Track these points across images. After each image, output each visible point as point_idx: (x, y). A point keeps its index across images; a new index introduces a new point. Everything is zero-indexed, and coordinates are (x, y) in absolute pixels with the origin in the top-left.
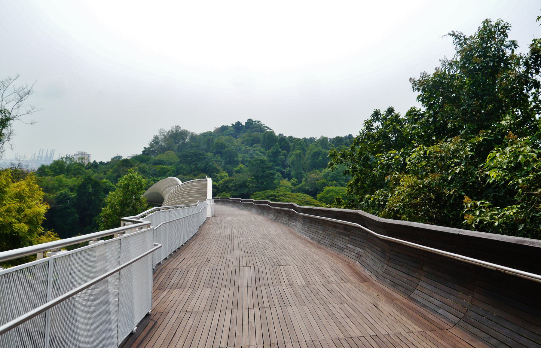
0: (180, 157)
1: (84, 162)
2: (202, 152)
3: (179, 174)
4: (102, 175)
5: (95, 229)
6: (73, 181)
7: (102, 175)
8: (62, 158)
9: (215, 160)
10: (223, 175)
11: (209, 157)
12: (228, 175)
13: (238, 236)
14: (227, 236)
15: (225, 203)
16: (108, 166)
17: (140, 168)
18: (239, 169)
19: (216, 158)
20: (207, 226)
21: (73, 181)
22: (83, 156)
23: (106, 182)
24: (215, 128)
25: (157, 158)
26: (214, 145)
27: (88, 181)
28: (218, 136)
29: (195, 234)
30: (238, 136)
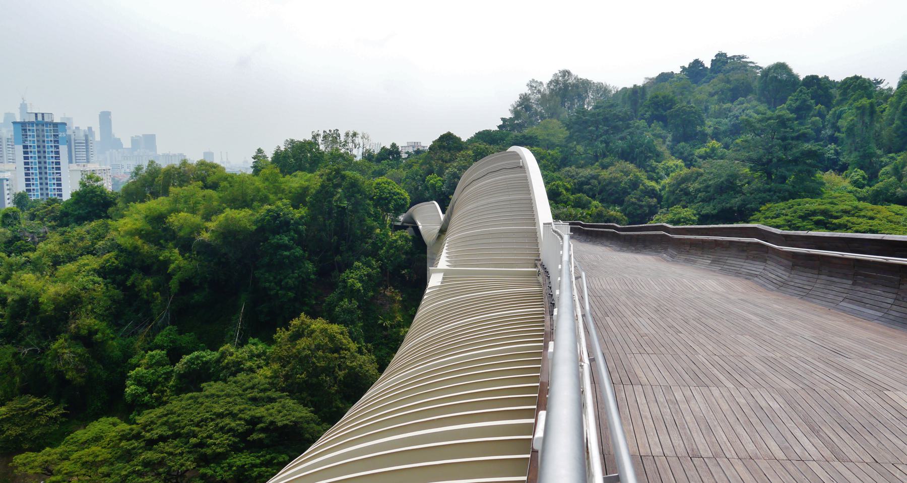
12: (683, 164)
18: (708, 150)
24: (646, 78)
26: (647, 102)
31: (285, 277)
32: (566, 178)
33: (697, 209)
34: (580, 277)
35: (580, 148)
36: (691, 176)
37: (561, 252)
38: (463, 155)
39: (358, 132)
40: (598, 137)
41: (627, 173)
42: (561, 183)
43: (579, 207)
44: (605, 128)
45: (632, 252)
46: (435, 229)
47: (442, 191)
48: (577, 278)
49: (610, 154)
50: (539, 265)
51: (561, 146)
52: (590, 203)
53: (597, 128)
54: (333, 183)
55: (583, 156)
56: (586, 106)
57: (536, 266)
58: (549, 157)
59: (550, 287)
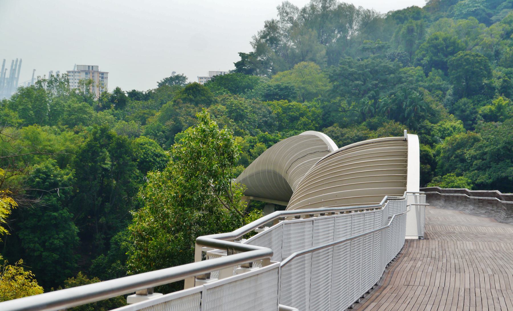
0: (332, 79)
1: (91, 91)
2: (391, 65)
3: (331, 124)
4: (134, 126)
5: (119, 262)
6: (66, 140)
7: (134, 126)
8: (39, 82)
9: (427, 84)
10: (448, 125)
11: (412, 76)
12: (461, 126)
13: (495, 295)
14: (462, 293)
15: (453, 201)
16: (149, 102)
17: (229, 107)
18: (493, 108)
19: (431, 81)
20: (406, 265)
21: (66, 140)
22: (90, 77)
23: (146, 143)
25: (273, 82)
26: (425, 44)
27: (103, 141)
28: (436, 19)
29: (376, 285)
30: (493, 18)
31: (50, 238)
33: (472, 178)
36: (467, 142)
53: (365, 81)
54: (99, 143)
58: (310, 114)
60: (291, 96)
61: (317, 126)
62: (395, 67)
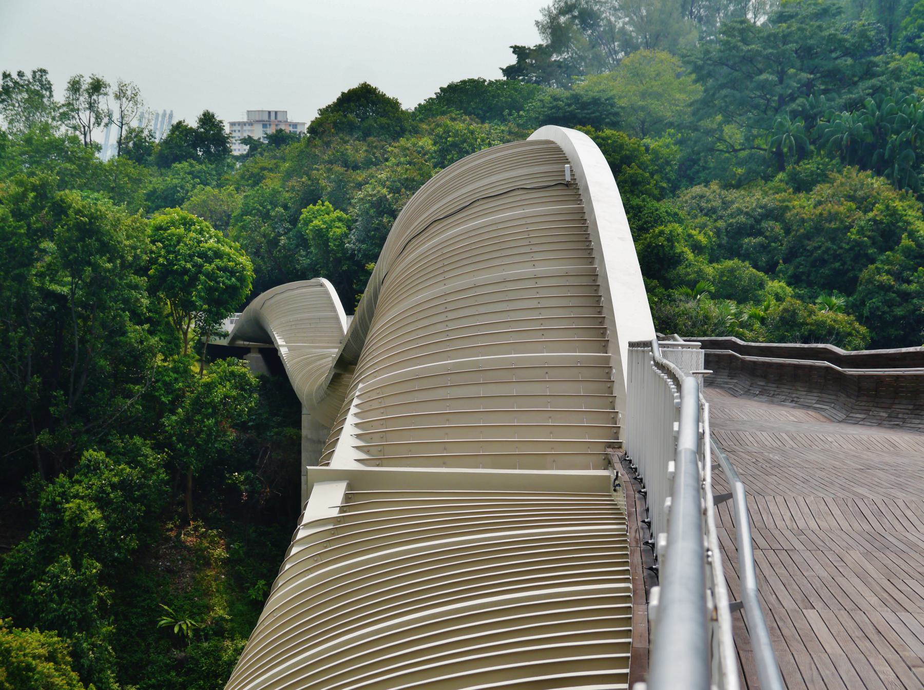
32: (695, 217)
34: (730, 496)
35: (734, 133)
37: (676, 426)
38: (405, 149)
39: (107, 79)
40: (783, 101)
41: (864, 203)
42: (680, 230)
43: (729, 297)
44: (805, 76)
45: (880, 425)
46: (323, 357)
47: (344, 251)
48: (719, 500)
49: (819, 149)
50: (616, 460)
51: (679, 128)
52: (761, 285)
53: (782, 75)
54: (29, 225)
55: (743, 154)
56: (750, 16)
57: (608, 464)
58: (647, 158)
59: (649, 524)
60: (607, 120)
61: (665, 185)
62: (856, 39)
